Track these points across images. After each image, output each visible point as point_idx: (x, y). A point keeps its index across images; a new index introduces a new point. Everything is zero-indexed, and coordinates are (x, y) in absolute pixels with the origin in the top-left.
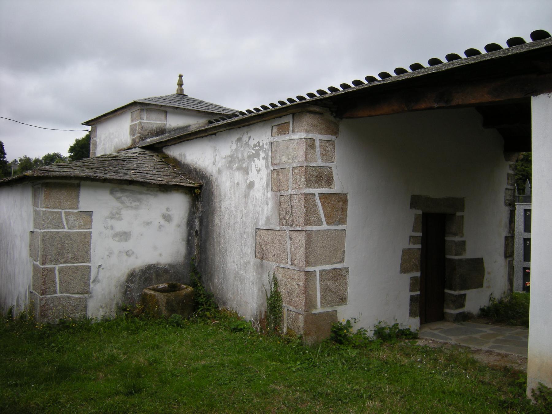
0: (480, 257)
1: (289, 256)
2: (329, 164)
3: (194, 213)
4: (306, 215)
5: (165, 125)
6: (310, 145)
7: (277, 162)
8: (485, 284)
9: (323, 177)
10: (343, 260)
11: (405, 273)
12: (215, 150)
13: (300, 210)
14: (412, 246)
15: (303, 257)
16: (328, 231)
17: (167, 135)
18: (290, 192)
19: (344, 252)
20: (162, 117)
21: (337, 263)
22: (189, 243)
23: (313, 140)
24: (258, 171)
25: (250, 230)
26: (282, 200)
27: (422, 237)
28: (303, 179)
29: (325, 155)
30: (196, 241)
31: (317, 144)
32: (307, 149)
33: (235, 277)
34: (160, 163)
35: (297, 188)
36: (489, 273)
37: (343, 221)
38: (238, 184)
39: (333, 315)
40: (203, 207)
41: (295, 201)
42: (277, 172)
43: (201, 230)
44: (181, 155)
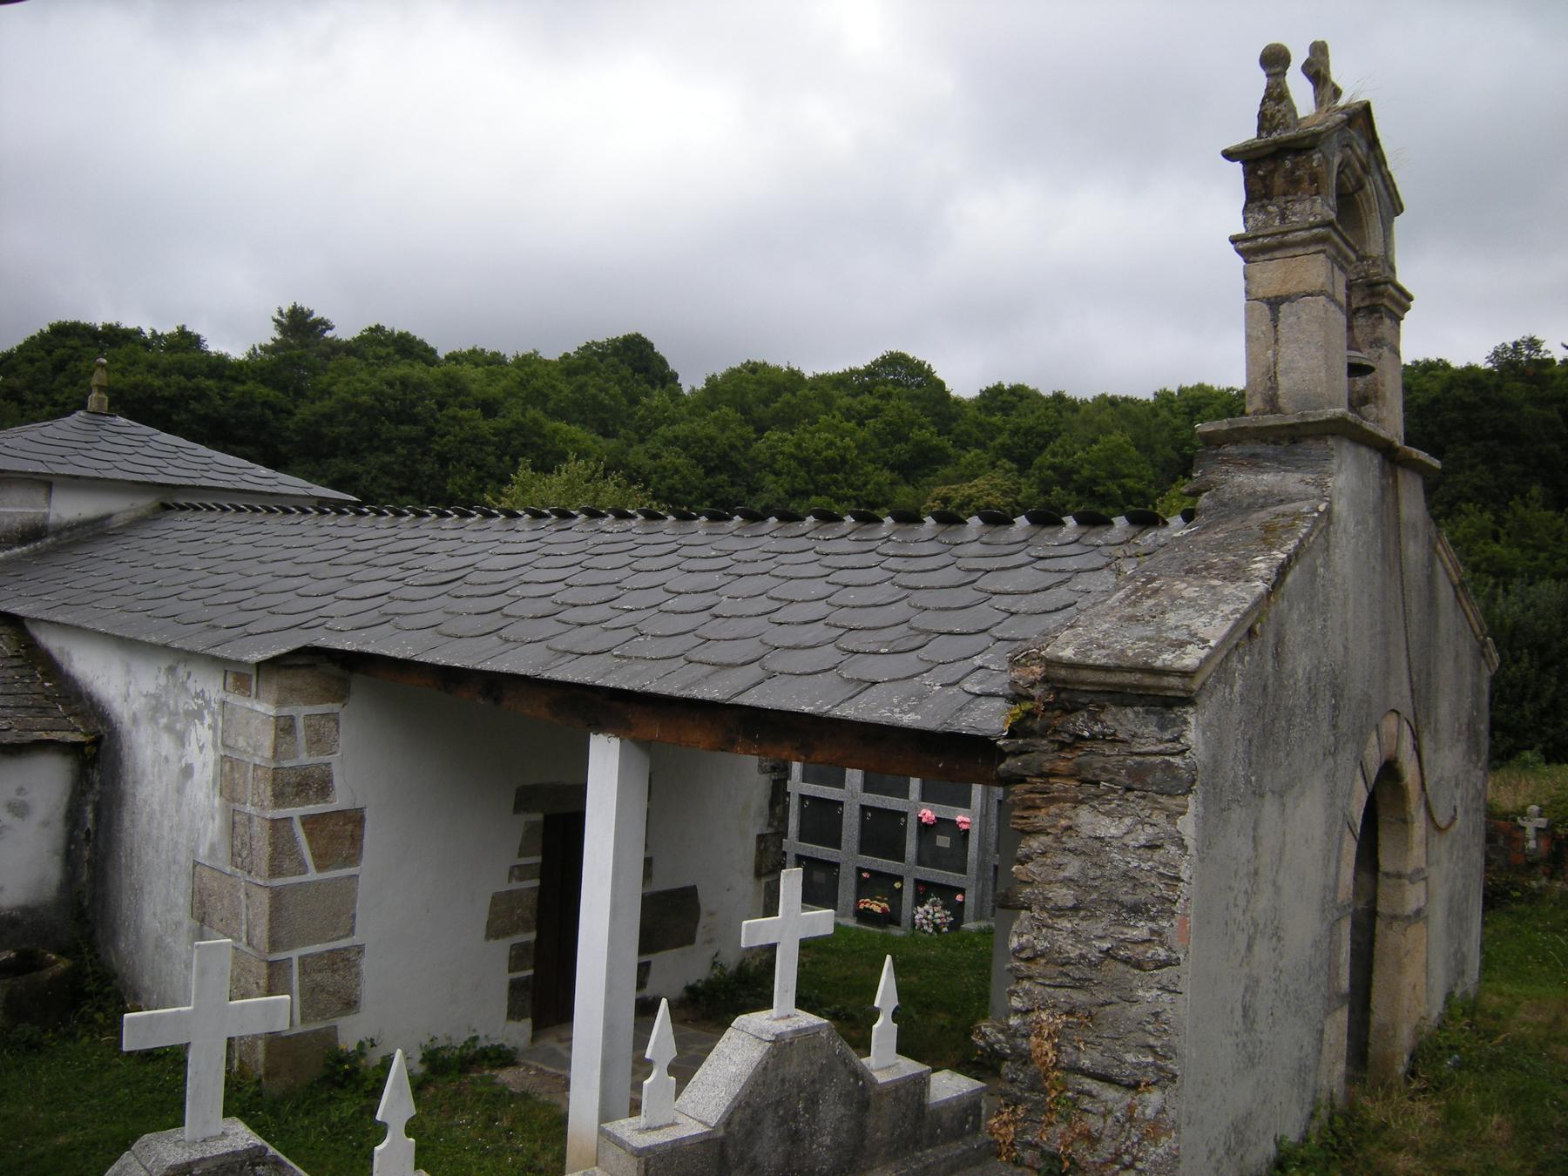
0: (689, 883)
1: (244, 927)
2: (326, 759)
3: (83, 793)
4: (272, 858)
5: (46, 516)
6: (285, 728)
7: (230, 742)
8: (699, 937)
9: (315, 784)
10: (352, 931)
11: (497, 938)
12: (128, 671)
13: (262, 848)
14: (517, 885)
15: (265, 934)
16: (320, 882)
17: (49, 540)
18: (249, 808)
19: (354, 916)
20: (39, 497)
21: (338, 938)
22: (70, 858)
23: (292, 718)
24: (201, 748)
25: (184, 859)
26: (237, 818)
27: (543, 864)
28: (269, 792)
29: (318, 741)
30: (86, 853)
31: (300, 724)
32: (277, 736)
33: (157, 947)
34: (16, 662)
35: (259, 808)
36: (712, 914)
37: (353, 859)
38: (166, 758)
39: (330, 1035)
40: (102, 782)
41: (256, 828)
42: (229, 764)
43: (96, 832)
44: (61, 649)
